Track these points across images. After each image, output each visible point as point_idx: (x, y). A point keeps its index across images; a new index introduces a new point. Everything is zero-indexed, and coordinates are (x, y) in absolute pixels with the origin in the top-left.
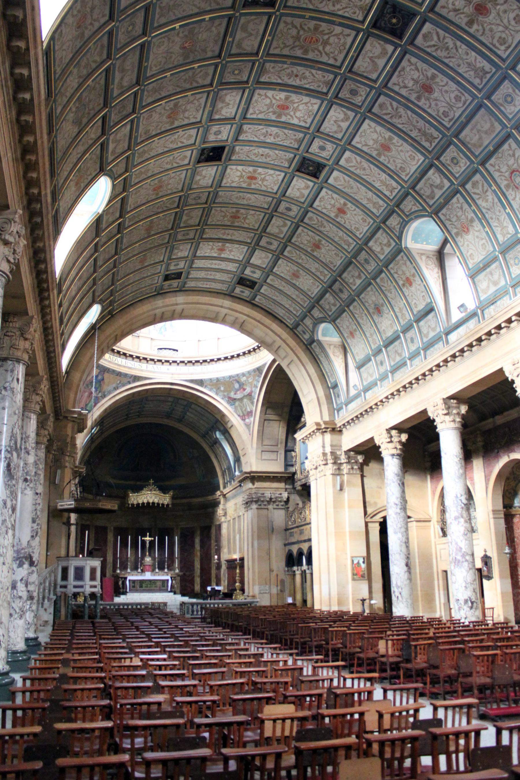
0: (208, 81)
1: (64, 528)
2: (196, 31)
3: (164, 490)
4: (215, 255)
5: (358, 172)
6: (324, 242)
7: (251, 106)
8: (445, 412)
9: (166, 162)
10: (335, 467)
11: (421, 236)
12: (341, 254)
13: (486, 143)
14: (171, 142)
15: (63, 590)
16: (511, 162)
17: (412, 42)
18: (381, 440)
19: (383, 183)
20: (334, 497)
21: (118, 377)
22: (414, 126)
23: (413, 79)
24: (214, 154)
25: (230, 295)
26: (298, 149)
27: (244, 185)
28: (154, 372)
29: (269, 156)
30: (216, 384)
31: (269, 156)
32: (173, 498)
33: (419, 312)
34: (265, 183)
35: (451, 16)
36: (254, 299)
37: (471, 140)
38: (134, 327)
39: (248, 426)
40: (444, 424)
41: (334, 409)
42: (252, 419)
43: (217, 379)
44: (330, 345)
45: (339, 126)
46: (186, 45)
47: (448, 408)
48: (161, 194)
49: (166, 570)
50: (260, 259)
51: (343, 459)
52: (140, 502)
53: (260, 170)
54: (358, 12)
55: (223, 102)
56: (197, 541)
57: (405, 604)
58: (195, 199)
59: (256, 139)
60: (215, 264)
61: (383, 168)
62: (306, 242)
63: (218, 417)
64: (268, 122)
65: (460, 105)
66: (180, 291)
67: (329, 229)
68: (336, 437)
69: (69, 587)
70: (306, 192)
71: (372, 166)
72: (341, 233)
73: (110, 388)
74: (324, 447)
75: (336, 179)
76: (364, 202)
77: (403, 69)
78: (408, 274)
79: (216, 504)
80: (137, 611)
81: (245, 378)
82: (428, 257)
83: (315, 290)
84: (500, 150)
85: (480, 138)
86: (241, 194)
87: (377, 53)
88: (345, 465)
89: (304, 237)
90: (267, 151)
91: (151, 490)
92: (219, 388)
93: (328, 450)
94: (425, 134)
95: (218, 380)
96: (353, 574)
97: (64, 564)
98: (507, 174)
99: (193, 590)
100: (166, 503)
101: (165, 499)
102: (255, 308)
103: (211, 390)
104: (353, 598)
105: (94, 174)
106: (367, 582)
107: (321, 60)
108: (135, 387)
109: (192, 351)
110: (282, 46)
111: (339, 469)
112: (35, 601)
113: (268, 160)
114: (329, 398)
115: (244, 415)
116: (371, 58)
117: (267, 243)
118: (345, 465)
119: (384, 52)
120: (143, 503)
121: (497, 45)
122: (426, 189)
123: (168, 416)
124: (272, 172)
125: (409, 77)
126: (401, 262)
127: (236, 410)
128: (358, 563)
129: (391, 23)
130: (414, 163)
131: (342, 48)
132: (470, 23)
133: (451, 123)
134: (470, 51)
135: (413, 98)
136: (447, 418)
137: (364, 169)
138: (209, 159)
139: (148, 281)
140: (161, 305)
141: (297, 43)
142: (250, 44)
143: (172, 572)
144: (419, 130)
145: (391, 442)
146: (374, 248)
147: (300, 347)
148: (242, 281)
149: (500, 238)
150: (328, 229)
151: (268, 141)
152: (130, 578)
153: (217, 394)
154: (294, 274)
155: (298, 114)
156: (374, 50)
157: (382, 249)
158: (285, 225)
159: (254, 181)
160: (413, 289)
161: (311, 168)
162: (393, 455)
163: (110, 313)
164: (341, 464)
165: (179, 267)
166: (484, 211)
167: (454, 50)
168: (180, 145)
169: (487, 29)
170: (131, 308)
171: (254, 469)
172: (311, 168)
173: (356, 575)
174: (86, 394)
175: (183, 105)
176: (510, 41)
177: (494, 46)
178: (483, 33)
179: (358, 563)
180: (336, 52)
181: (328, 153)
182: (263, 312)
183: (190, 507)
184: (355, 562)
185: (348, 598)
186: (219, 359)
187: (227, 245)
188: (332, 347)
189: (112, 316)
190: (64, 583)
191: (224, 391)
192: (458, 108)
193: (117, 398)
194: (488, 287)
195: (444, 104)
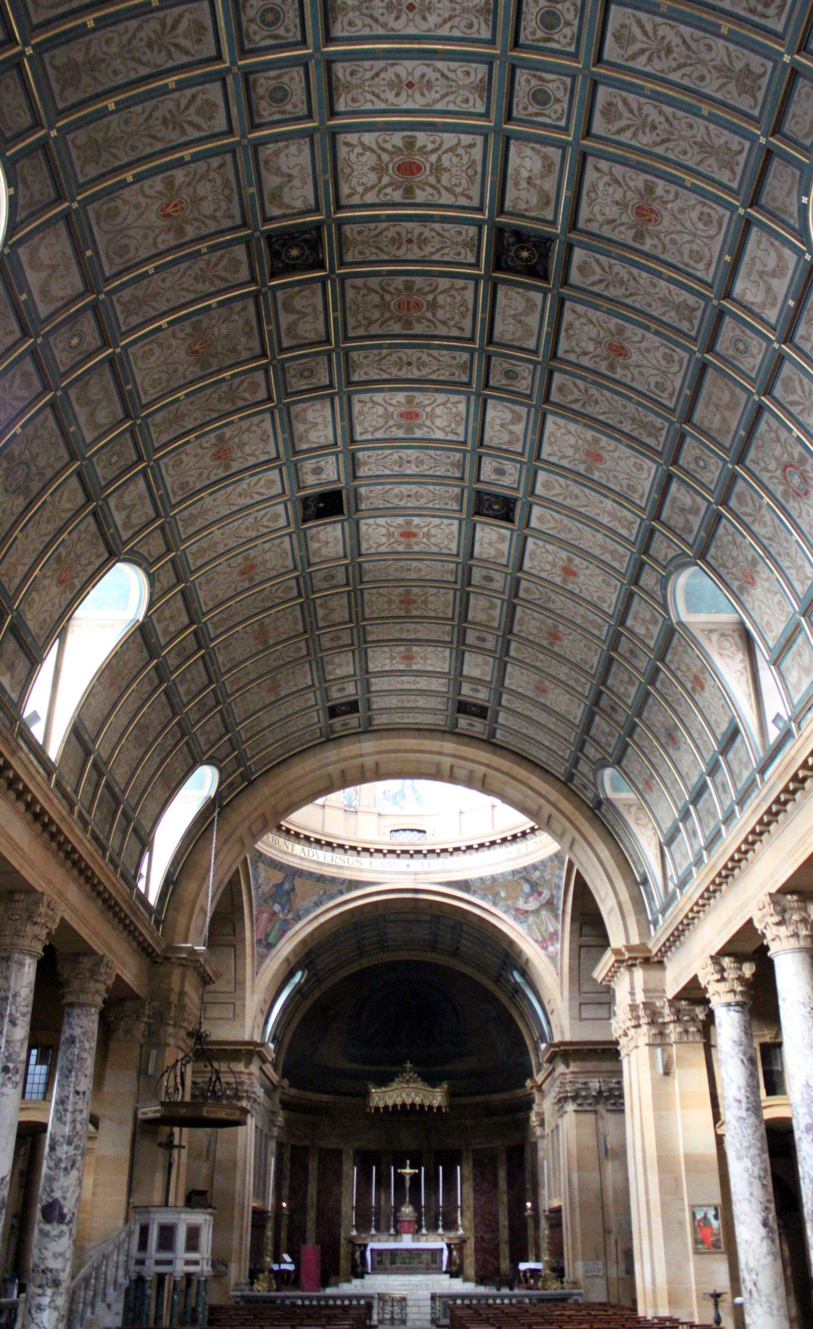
0: (262, 394)
1: (161, 1153)
2: (205, 325)
3: (432, 1080)
4: (402, 667)
5: (568, 502)
6: (561, 628)
7: (356, 422)
8: (777, 919)
9: (242, 527)
10: (654, 1031)
11: (694, 600)
12: (594, 647)
13: (733, 427)
14: (240, 495)
15: (138, 1268)
16: (778, 452)
17: (565, 282)
18: (708, 977)
19: (613, 515)
20: (654, 1088)
21: (320, 884)
22: (622, 414)
23: (591, 339)
24: (328, 504)
25: (452, 733)
26: (462, 479)
27: (401, 548)
28: (383, 872)
29: (422, 496)
30: (489, 886)
31: (422, 496)
32: (451, 1095)
33: (724, 735)
34: (433, 540)
35: (606, 231)
36: (494, 736)
37: (711, 423)
38: (295, 798)
39: (552, 958)
40: (777, 942)
41: (649, 922)
42: (558, 946)
43: (481, 879)
44: (630, 806)
45: (511, 433)
46: (197, 348)
47: (783, 911)
48: (258, 579)
49: (440, 1231)
50: (477, 666)
51: (667, 1015)
52: (390, 1103)
53: (416, 520)
54: (471, 98)
55: (305, 421)
56: (502, 1173)
57: (766, 1306)
58: (325, 580)
59: (388, 472)
60: (407, 682)
61: (603, 489)
62: (535, 631)
63: (505, 945)
64: (391, 443)
65: (675, 368)
66: (365, 732)
67: (559, 603)
68: (655, 974)
69: (147, 1262)
70: (504, 547)
71: (586, 490)
72: (581, 611)
73: (306, 903)
74: (632, 993)
75: (540, 519)
76: (597, 552)
77: (570, 325)
78: (694, 670)
79: (527, 1104)
80: (513, 1310)
81: (537, 873)
82: (723, 635)
83: (578, 713)
84: (758, 435)
85: (724, 420)
86: (401, 563)
87: (520, 310)
88: (671, 1026)
89: (529, 623)
90: (414, 488)
91: (408, 1082)
92: (497, 894)
93: (640, 998)
94: (643, 425)
95: (493, 879)
96: (696, 1242)
97: (143, 1219)
98: (779, 473)
99: (498, 1269)
100: (436, 1103)
101: (436, 1098)
102: (499, 751)
103: (483, 898)
104: (697, 1291)
105: (97, 563)
106: (725, 1256)
107: (436, 333)
108: (353, 900)
109: (415, 832)
110: (365, 322)
111: (661, 1034)
112: (62, 1289)
113: (422, 501)
114: (638, 903)
115: (544, 940)
116: (514, 317)
117: (478, 638)
118: (671, 1026)
119: (530, 305)
120: (395, 1106)
121: (692, 263)
122: (676, 517)
123: (433, 946)
124: (436, 521)
125: (585, 337)
126: (680, 649)
127: (530, 932)
128: (705, 1217)
129: (521, 259)
130: (645, 476)
131: (463, 309)
132: (639, 236)
133: (674, 400)
134: (655, 280)
135: (603, 368)
136: (783, 931)
137: (577, 497)
138: (320, 514)
139: (303, 722)
140: (334, 759)
141: (387, 315)
142: (311, 328)
143: (452, 1234)
144: (633, 420)
145: (722, 979)
146: (636, 630)
147: (582, 814)
148: (463, 707)
149: (799, 589)
150: (559, 604)
151: (408, 472)
152: (372, 1245)
153: (495, 904)
154: (537, 688)
155: (438, 422)
156: (514, 304)
157: (648, 629)
158: (492, 606)
159: (414, 540)
160: (707, 694)
161: (496, 507)
162: (729, 1005)
163: (244, 776)
164: (664, 1024)
165: (346, 693)
166: (766, 542)
167: (632, 283)
168: (258, 498)
169: (667, 240)
170: (283, 767)
171: (568, 1038)
172: (499, 507)
173: (702, 1242)
174: (265, 916)
175: (232, 437)
176: (707, 253)
177: (687, 265)
178: (664, 248)
179: (705, 1217)
180: (457, 318)
181: (512, 478)
182: (513, 757)
183: (490, 1111)
184: (699, 1216)
185: (688, 1291)
186: (493, 843)
187: (415, 648)
188: (633, 809)
189: (251, 783)
190: (140, 1255)
191: (505, 899)
192: (675, 374)
193: (322, 920)
194: (800, 679)
195: (653, 372)
